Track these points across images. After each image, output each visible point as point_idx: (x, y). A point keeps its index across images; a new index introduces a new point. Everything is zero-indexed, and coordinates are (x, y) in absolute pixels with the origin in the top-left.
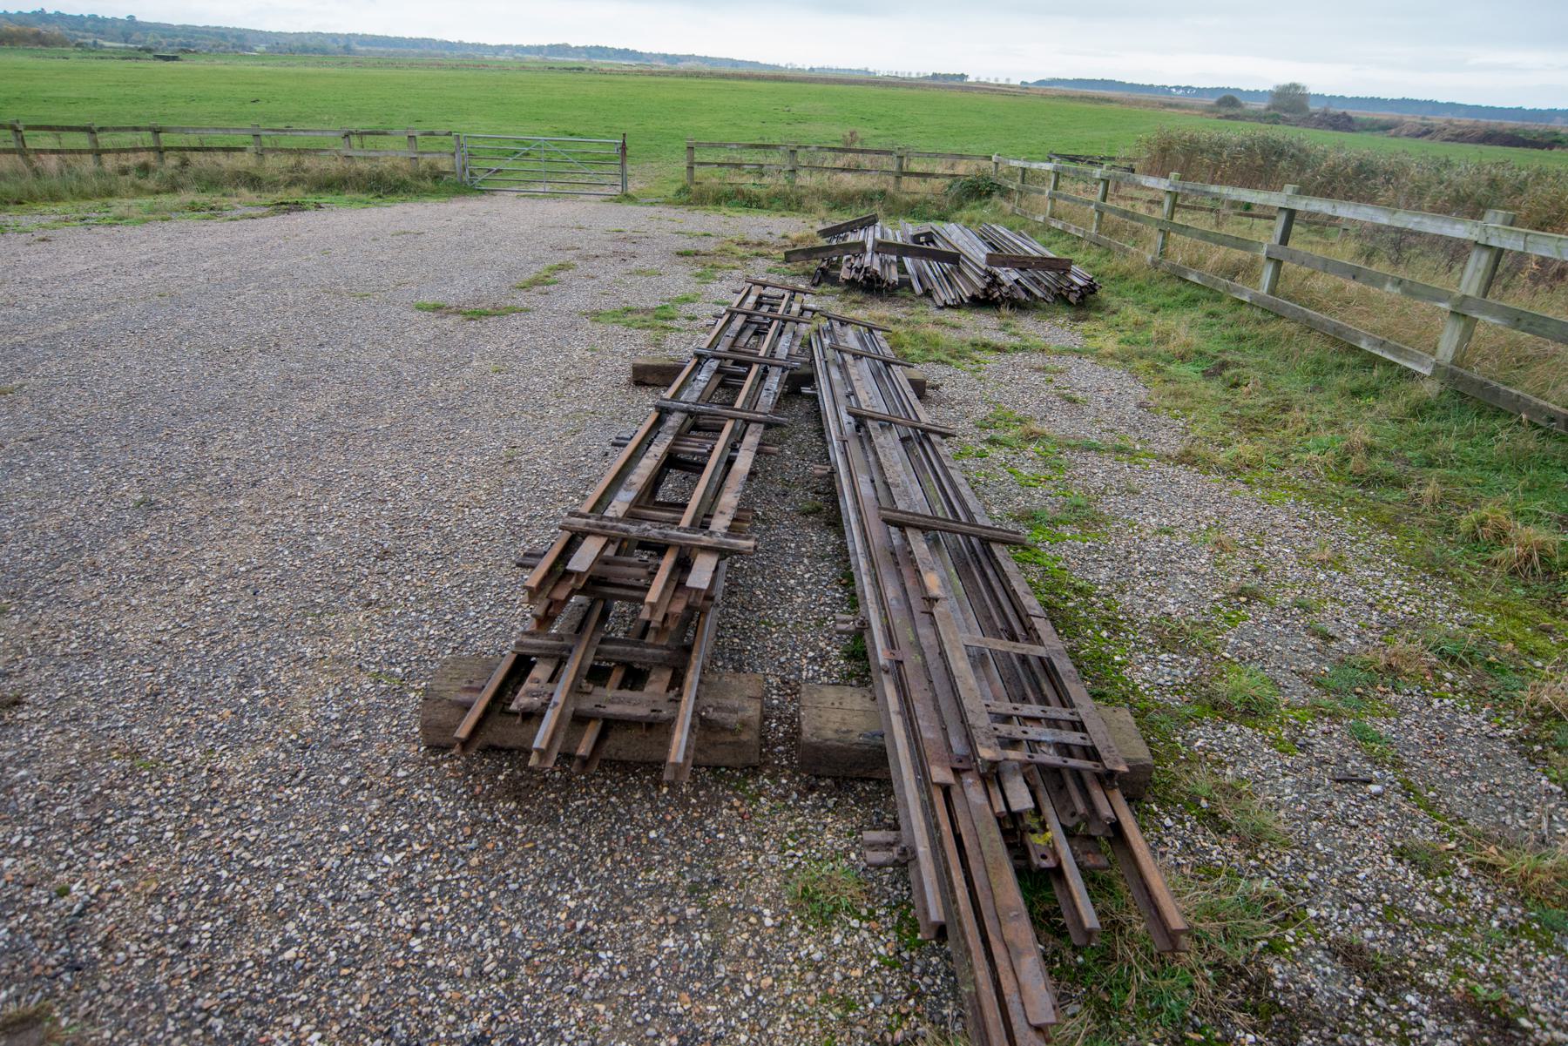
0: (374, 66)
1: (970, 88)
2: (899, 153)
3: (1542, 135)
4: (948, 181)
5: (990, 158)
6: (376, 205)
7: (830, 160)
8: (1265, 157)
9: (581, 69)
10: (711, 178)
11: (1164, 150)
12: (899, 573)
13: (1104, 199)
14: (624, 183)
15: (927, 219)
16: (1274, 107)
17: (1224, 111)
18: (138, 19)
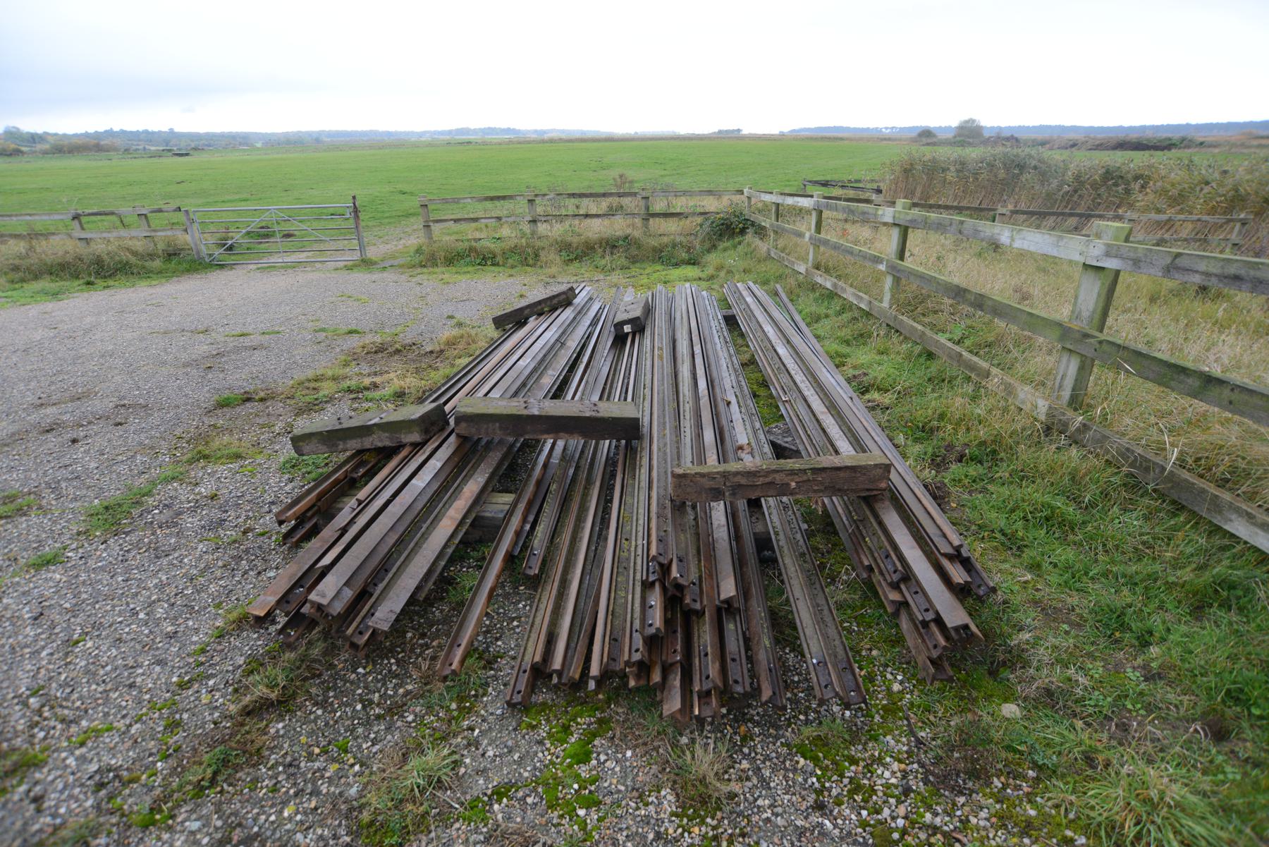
0: (325, 151)
1: (744, 138)
2: (644, 194)
3: (1160, 141)
4: (699, 220)
5: (741, 192)
6: (88, 291)
7: (570, 206)
8: (1007, 168)
9: (469, 143)
10: (445, 236)
11: (906, 171)
12: (700, 561)
13: (901, 255)
14: (362, 248)
15: (677, 265)
16: (960, 136)
17: (924, 140)
18: (176, 130)
